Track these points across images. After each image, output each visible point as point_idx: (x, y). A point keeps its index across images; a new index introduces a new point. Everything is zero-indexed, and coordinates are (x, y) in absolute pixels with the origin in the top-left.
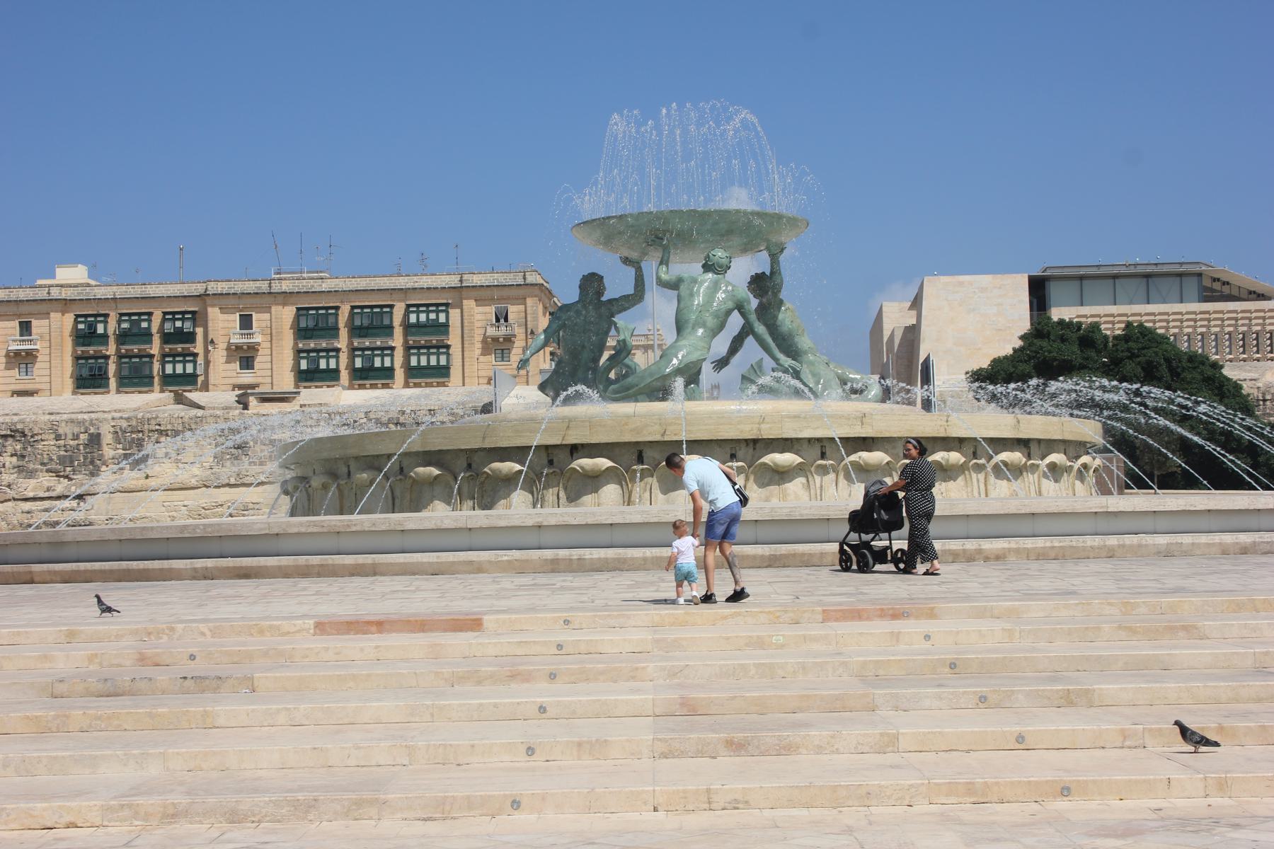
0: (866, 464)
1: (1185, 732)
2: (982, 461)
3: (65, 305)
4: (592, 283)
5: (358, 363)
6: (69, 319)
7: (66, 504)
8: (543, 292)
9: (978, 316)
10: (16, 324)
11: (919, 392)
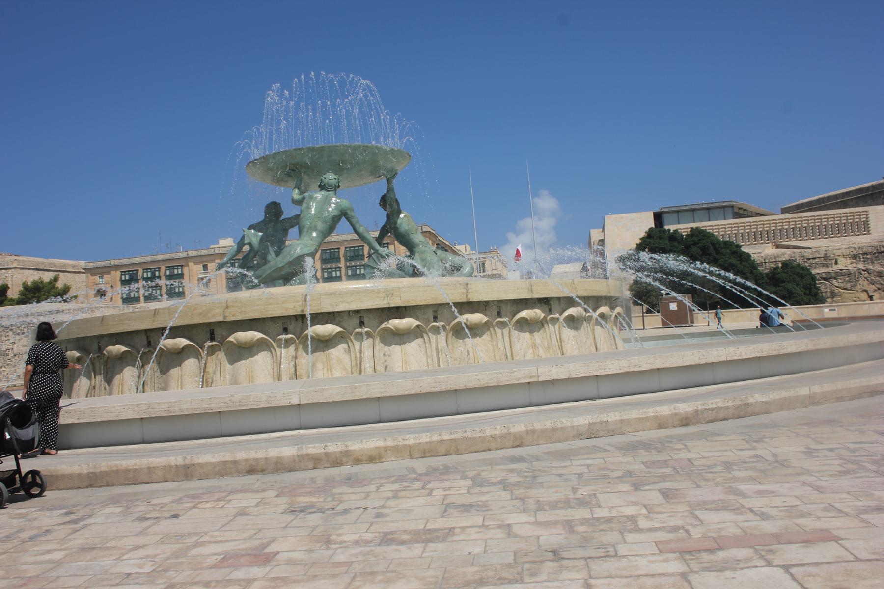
0: (397, 329)
2: (506, 319)
10: (201, 266)
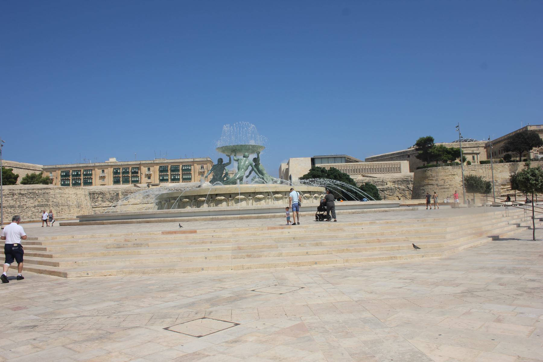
1: (414, 246)
3: (111, 166)
4: (220, 160)
5: (172, 178)
6: (112, 169)
7: (111, 208)
8: (211, 162)
9: (300, 166)
11: (289, 182)
